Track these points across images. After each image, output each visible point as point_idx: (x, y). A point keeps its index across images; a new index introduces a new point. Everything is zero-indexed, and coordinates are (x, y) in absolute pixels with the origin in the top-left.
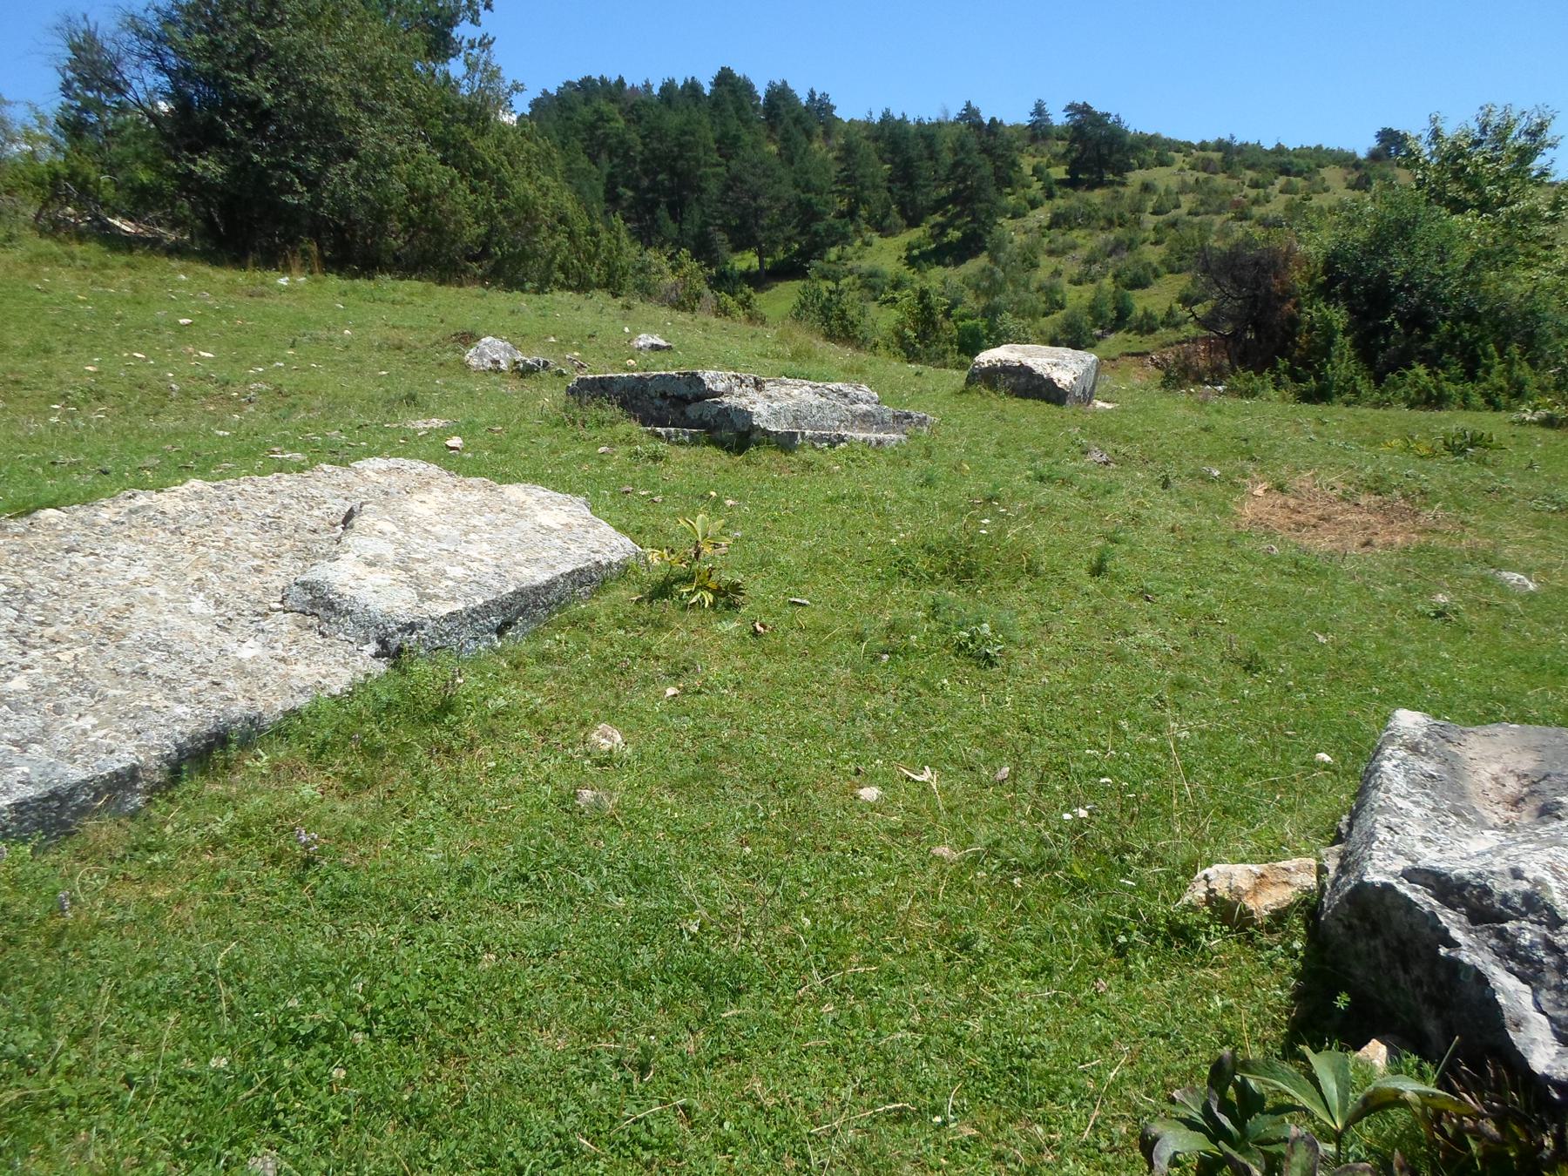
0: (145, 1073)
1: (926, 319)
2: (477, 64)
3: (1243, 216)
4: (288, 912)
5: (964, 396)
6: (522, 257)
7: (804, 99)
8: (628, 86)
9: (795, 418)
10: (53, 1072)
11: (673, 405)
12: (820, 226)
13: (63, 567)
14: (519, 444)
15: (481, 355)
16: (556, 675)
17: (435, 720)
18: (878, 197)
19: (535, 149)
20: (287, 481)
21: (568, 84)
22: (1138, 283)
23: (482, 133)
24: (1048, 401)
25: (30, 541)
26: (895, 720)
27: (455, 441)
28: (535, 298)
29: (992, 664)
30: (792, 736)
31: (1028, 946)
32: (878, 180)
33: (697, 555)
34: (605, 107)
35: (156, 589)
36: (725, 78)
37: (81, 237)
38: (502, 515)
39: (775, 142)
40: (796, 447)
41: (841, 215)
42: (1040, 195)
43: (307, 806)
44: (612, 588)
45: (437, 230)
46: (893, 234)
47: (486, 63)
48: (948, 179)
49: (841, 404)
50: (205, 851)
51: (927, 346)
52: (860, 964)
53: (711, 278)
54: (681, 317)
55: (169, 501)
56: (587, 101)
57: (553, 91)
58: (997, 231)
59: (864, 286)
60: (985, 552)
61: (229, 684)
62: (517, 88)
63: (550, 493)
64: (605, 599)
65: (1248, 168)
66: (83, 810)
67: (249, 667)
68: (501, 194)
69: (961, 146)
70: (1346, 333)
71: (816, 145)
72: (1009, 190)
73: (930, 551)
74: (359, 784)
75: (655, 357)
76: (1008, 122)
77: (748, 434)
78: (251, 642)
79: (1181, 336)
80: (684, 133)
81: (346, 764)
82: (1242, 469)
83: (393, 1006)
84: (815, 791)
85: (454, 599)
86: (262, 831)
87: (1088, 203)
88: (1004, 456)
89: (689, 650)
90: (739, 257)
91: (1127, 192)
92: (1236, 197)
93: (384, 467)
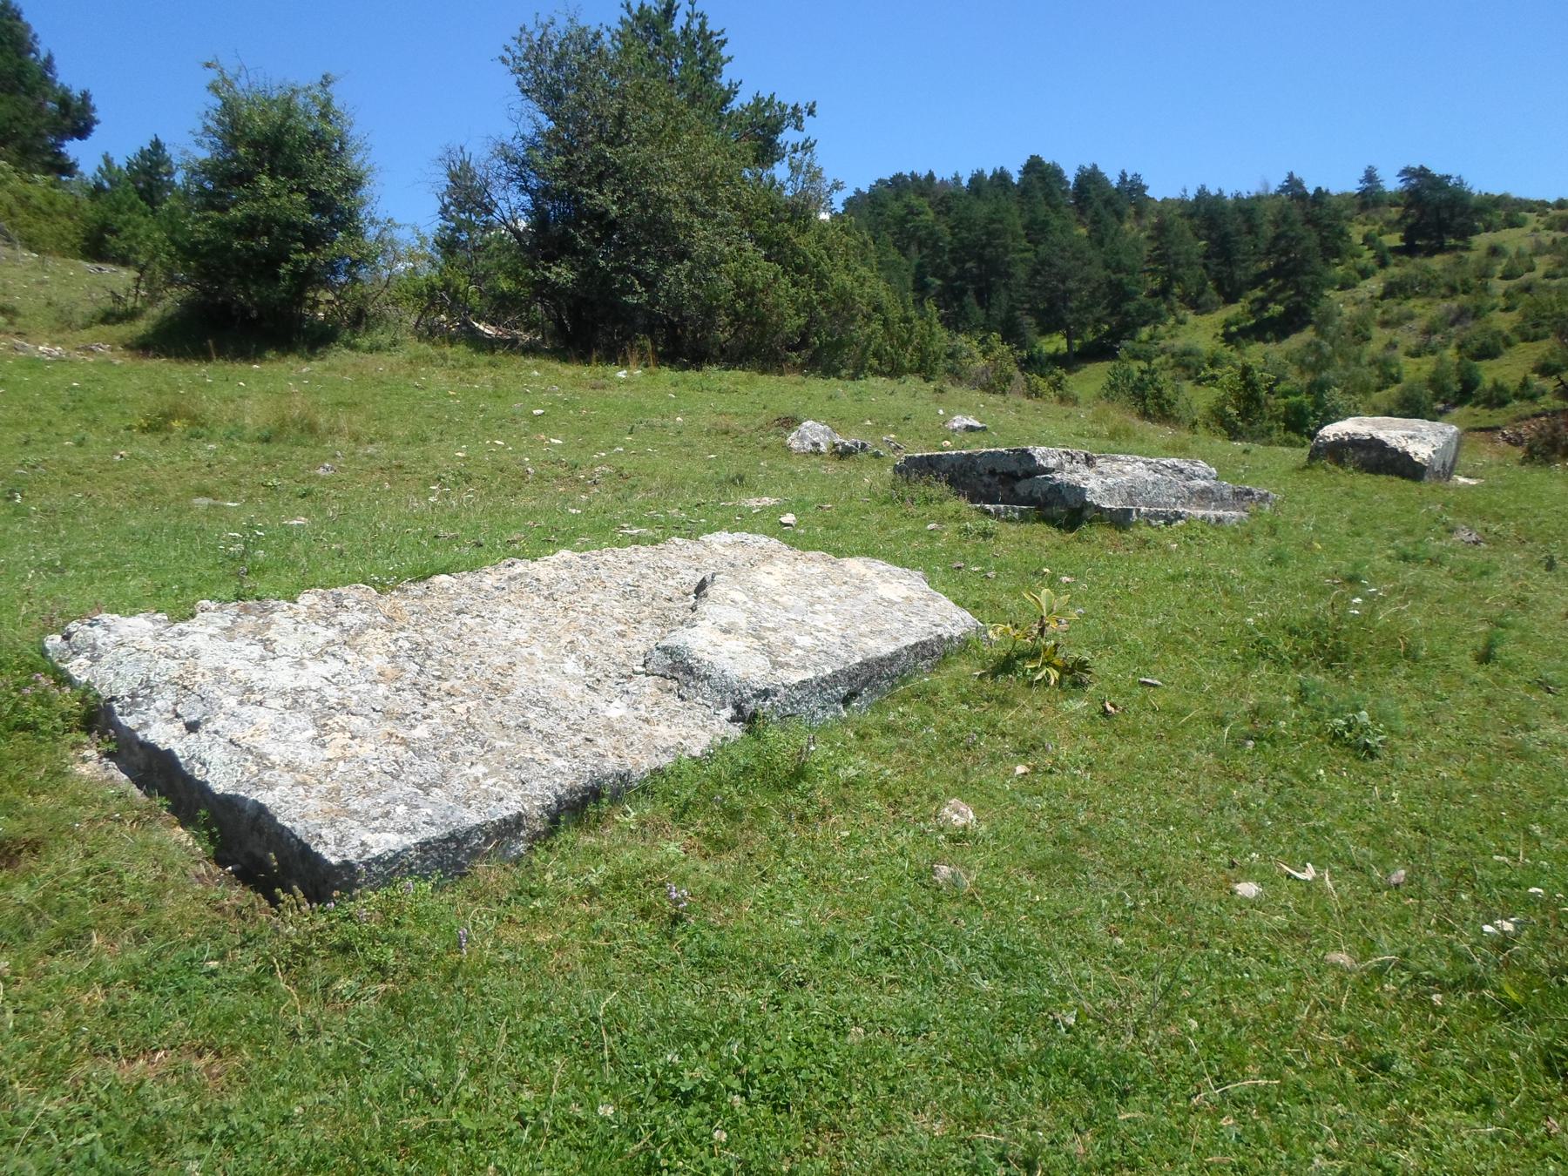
0: (536, 1114)
1: (1249, 395)
2: (800, 167)
4: (658, 967)
5: (1308, 472)
6: (839, 345)
7: (1114, 180)
8: (938, 180)
9: (1130, 495)
10: (454, 1103)
11: (1002, 482)
12: (1131, 306)
13: (454, 627)
14: (850, 520)
15: (802, 438)
16: (901, 747)
17: (789, 786)
18: (1192, 275)
19: (854, 243)
20: (644, 553)
21: (880, 181)
22: (1487, 352)
23: (803, 230)
25: (427, 603)
26: (1267, 812)
27: (789, 518)
28: (850, 384)
29: (1372, 755)
30: (1154, 822)
31: (1458, 1073)
32: (1194, 258)
33: (1042, 631)
34: (915, 201)
35: (533, 650)
36: (1034, 166)
37: (452, 341)
38: (844, 587)
39: (1085, 225)
40: (1131, 525)
41: (1153, 294)
42: (1372, 264)
43: (673, 863)
44: (953, 662)
45: (761, 322)
46: (1208, 311)
47: (809, 165)
48: (1268, 253)
49: (1179, 480)
50: (581, 900)
51: (1251, 424)
52: (1261, 1076)
53: (1023, 361)
54: (992, 399)
55: (542, 569)
56: (898, 197)
57: (866, 190)
58: (1324, 304)
59: (1178, 365)
60: (1355, 635)
61: (600, 741)
62: (837, 186)
63: (889, 566)
64: (947, 673)
66: (475, 853)
67: (617, 726)
68: (820, 286)
69: (1283, 219)
71: (1127, 226)
73: (1292, 632)
74: (721, 846)
75: (970, 438)
76: (1334, 191)
78: (617, 702)
79: (1537, 409)
80: (992, 221)
81: (707, 824)
83: (767, 1072)
84: (1185, 882)
85: (804, 667)
86: (633, 885)
87: (1426, 270)
88: (1359, 535)
89: (1036, 729)
90: (1046, 340)
91: (1471, 256)
93: (729, 540)
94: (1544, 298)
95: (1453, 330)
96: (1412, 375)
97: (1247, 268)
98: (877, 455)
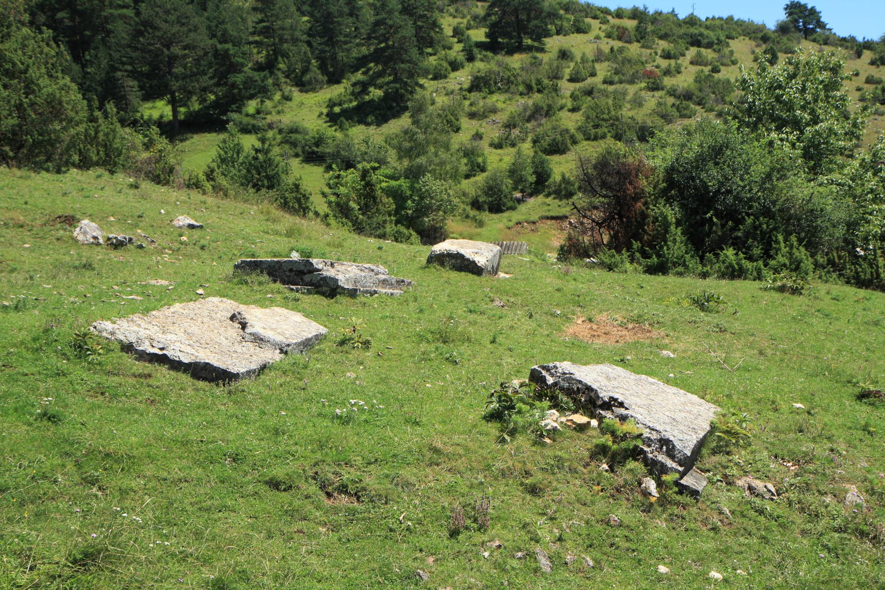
3: (655, 87)
5: (427, 270)
12: (238, 78)
15: (85, 233)
22: (557, 149)
24: (473, 273)
32: (298, 34)
41: (259, 67)
42: (461, 57)
46: (313, 90)
58: (419, 94)
65: (661, 38)
70: (678, 223)
72: (430, 50)
73: (432, 333)
77: (336, 289)
82: (573, 311)
90: (149, 105)
91: (545, 58)
92: (649, 67)
94: (603, 101)
95: (529, 125)
96: (495, 166)
97: (348, 50)
98: (141, 247)
